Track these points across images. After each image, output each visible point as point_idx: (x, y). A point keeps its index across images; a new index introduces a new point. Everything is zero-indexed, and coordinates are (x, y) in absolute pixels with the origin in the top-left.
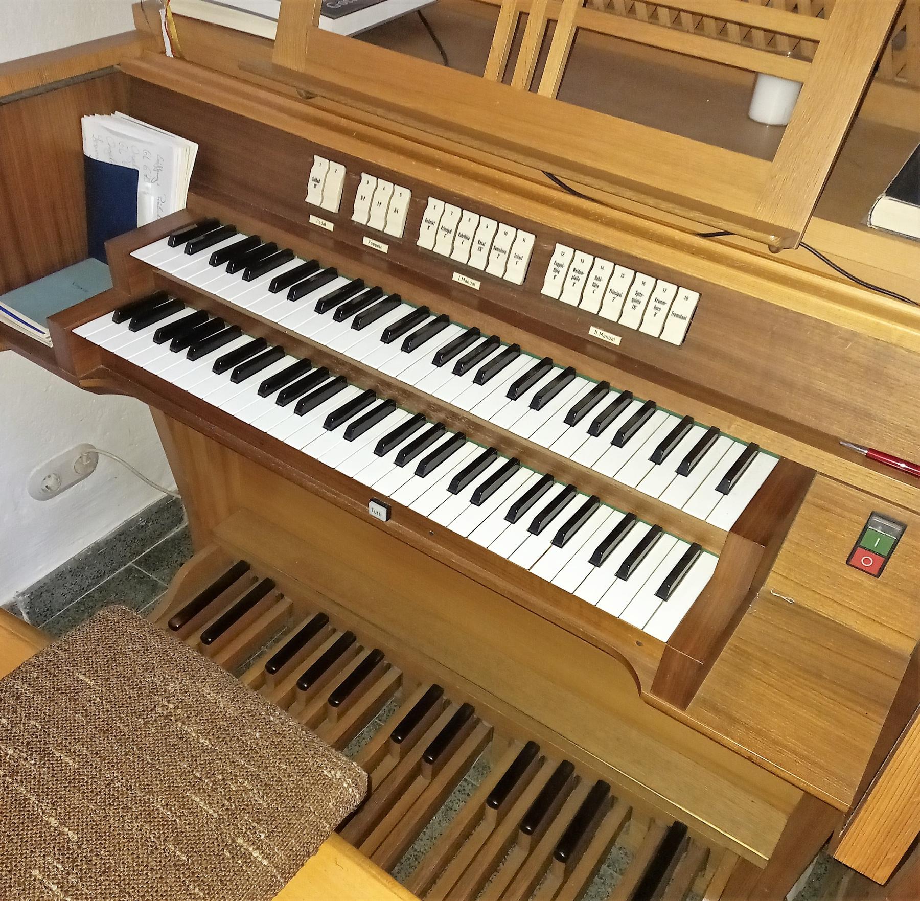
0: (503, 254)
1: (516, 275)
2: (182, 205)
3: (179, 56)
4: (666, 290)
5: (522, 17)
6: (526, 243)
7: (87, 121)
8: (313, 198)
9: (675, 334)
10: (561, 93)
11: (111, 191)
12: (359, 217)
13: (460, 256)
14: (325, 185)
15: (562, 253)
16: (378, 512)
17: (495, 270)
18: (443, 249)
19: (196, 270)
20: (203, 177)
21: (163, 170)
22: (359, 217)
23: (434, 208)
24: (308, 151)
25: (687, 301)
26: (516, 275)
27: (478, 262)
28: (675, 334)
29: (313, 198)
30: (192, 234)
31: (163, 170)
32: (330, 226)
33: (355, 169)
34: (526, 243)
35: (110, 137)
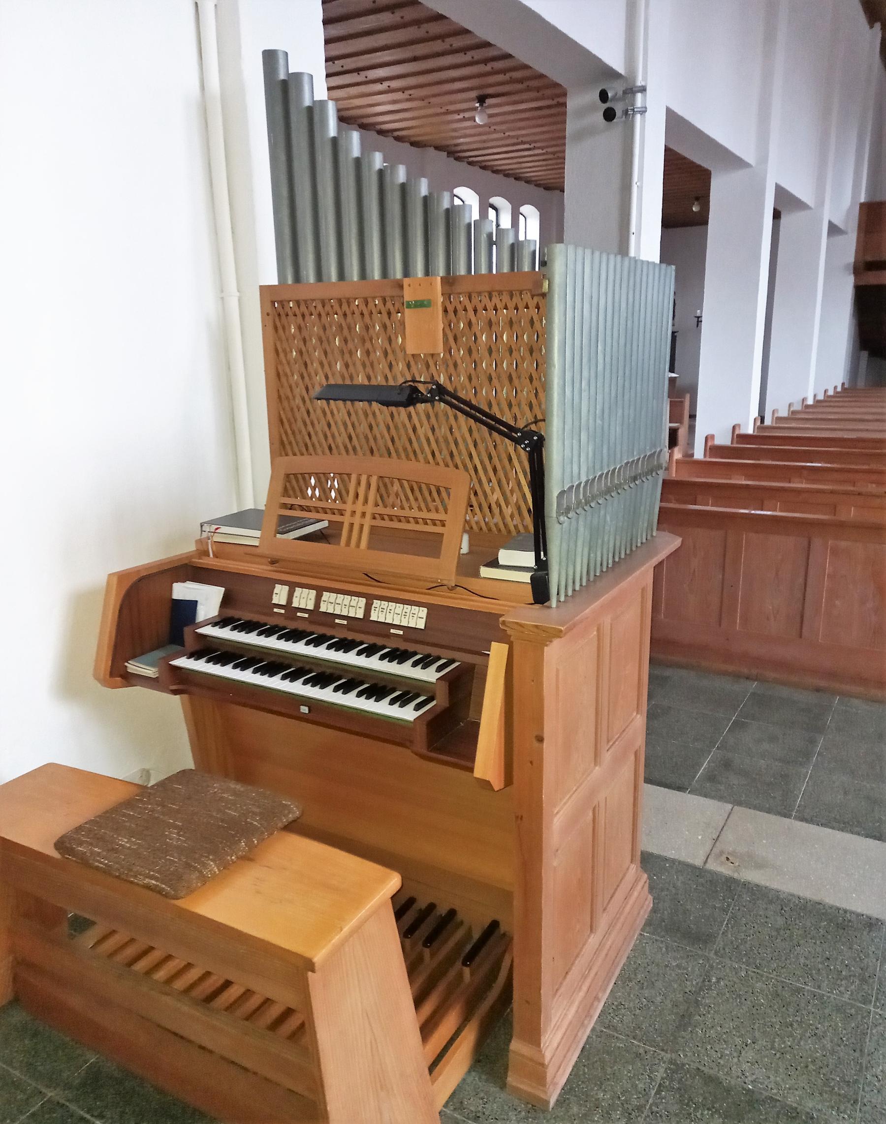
0: (353, 607)
1: (360, 615)
2: (216, 613)
3: (216, 556)
4: (415, 609)
5: (883, 407)
6: (362, 601)
7: (175, 585)
8: (275, 600)
9: (421, 625)
10: (370, 546)
11: (185, 611)
12: (295, 604)
13: (337, 612)
14: (280, 595)
15: (376, 603)
16: (304, 709)
17: (352, 615)
18: (330, 611)
19: (226, 633)
20: (226, 602)
21: (208, 599)
22: (295, 604)
23: (326, 595)
24: (272, 583)
25: (423, 612)
26: (360, 615)
27: (345, 613)
28: (421, 625)
29: (275, 600)
30: (222, 622)
31: (208, 599)
32: (283, 611)
33: (293, 586)
34: (362, 601)
35: (182, 591)
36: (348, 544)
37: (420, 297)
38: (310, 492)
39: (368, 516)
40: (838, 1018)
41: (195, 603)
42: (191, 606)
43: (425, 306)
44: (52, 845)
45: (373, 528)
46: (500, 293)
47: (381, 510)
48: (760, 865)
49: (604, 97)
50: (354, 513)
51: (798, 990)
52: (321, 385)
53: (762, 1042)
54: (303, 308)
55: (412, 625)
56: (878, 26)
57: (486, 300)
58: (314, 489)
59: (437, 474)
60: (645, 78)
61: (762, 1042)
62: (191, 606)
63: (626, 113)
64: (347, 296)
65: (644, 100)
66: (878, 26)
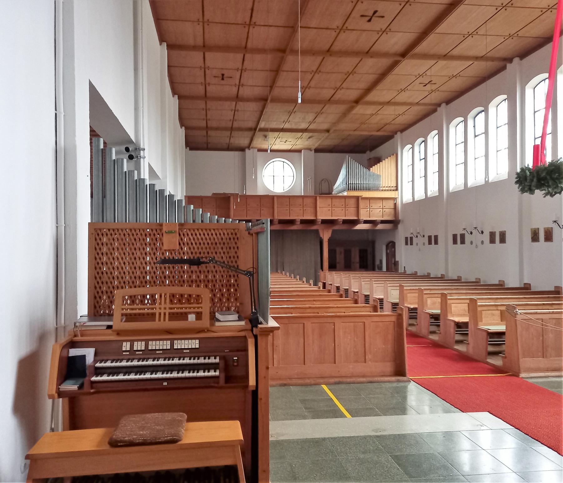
1: (169, 347)
4: (194, 341)
6: (169, 342)
9: (197, 346)
10: (169, 320)
12: (135, 349)
16: (165, 384)
20: (96, 354)
25: (197, 341)
26: (169, 347)
29: (124, 349)
31: (89, 353)
35: (73, 352)
36: (160, 320)
37: (170, 230)
38: (146, 302)
39: (167, 308)
40: (332, 463)
41: (85, 355)
42: (83, 357)
44: (107, 443)
45: (169, 314)
46: (218, 229)
48: (283, 435)
49: (127, 149)
50: (165, 308)
51: (318, 460)
52: (161, 258)
53: (318, 474)
54: (111, 231)
55: (194, 347)
58: (148, 300)
59: (194, 290)
60: (144, 145)
61: (318, 474)
62: (83, 358)
63: (137, 157)
64: (143, 228)
65: (144, 154)
66: (183, 128)
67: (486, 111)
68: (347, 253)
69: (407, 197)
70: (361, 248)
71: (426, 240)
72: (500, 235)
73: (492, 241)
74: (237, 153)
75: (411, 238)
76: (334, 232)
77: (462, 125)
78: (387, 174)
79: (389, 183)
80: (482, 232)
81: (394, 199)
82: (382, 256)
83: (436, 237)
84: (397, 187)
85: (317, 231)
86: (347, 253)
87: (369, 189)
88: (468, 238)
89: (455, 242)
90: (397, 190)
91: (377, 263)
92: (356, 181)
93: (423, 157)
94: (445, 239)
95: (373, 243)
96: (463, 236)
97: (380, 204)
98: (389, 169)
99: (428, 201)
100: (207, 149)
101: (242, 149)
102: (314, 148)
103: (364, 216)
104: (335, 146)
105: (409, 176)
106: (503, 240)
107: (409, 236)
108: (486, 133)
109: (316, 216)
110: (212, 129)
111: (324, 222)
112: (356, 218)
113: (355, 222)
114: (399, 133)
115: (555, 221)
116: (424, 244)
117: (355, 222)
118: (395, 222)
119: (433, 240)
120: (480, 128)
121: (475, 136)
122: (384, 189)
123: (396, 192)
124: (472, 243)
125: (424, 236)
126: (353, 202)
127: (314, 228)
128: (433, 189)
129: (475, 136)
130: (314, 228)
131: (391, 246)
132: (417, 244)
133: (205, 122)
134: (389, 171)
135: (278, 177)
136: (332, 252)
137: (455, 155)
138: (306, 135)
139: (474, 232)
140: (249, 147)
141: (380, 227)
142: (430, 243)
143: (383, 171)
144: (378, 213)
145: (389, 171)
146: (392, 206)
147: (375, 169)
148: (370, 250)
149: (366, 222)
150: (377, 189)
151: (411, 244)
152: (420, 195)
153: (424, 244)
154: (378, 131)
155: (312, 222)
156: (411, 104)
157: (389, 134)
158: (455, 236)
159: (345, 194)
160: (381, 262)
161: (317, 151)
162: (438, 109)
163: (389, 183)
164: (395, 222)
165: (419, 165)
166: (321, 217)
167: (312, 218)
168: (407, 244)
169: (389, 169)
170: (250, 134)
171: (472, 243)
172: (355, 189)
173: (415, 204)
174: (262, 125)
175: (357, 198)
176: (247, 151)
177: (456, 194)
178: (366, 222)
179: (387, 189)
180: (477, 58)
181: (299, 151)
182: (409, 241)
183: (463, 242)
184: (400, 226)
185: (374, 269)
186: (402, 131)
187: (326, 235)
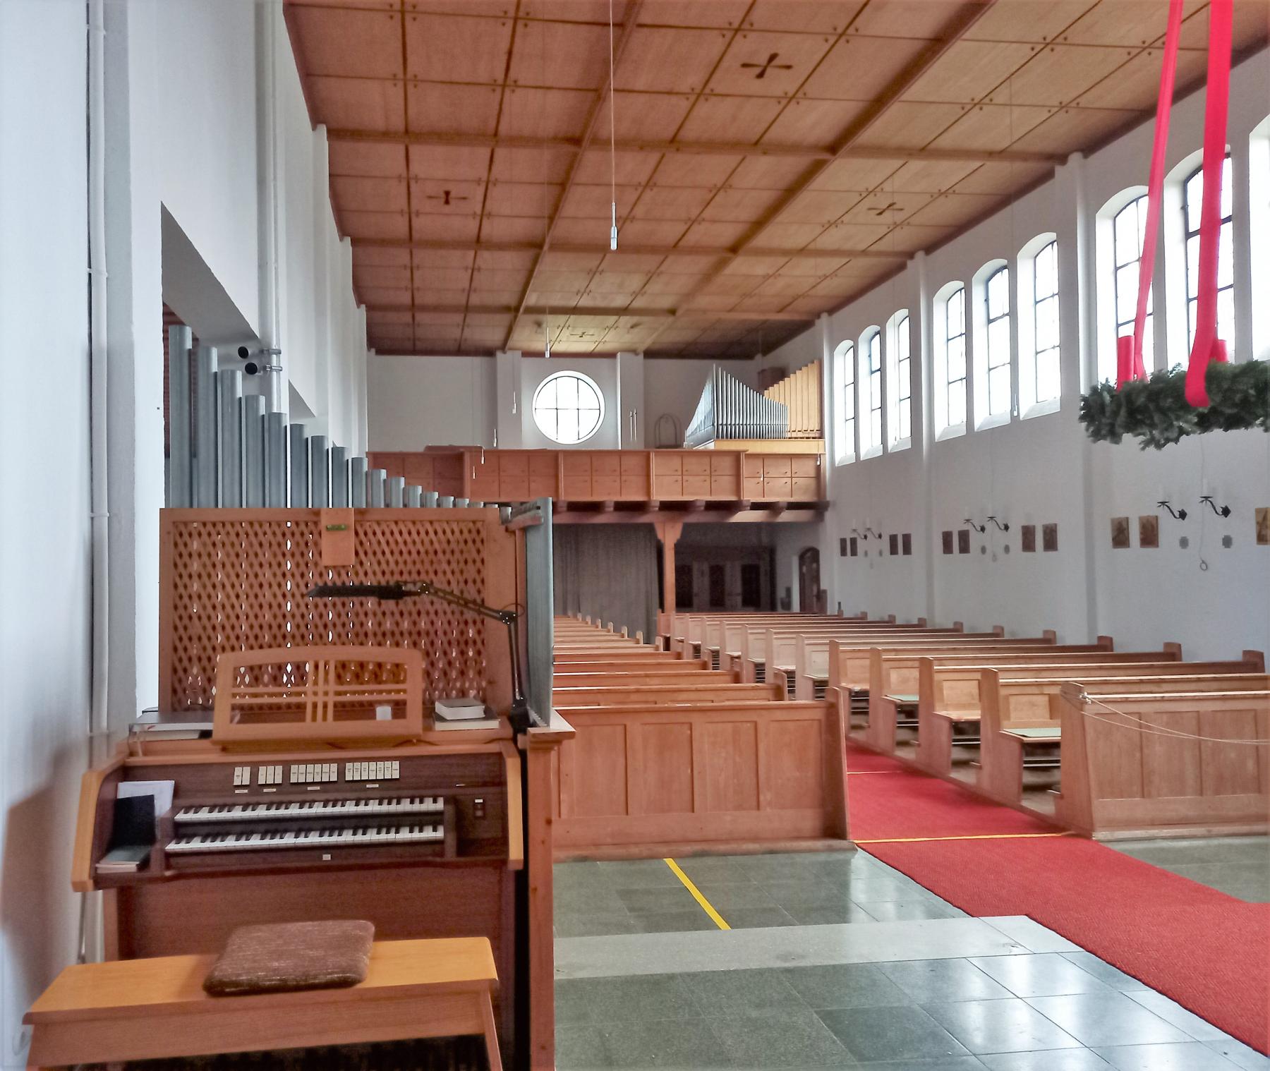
4: (388, 764)
6: (334, 767)
12: (261, 781)
17: (325, 779)
20: (177, 793)
25: (396, 764)
27: (318, 779)
29: (237, 782)
38: (285, 679)
39: (331, 694)
42: (149, 801)
43: (1265, 518)
44: (200, 988)
45: (335, 705)
47: (341, 688)
49: (243, 353)
56: (363, 307)
57: (428, 526)
58: (289, 676)
59: (387, 654)
60: (278, 343)
63: (265, 368)
65: (279, 361)
66: (363, 307)
67: (1012, 267)
68: (717, 574)
69: (843, 452)
70: (741, 564)
71: (885, 544)
72: (1045, 533)
73: (1028, 545)
74: (477, 361)
75: (854, 541)
76: (687, 527)
77: (1145, 202)
78: (799, 403)
79: (805, 422)
80: (1007, 528)
81: (816, 457)
82: (790, 578)
83: (907, 539)
84: (821, 430)
85: (650, 528)
86: (717, 574)
87: (761, 436)
88: (975, 540)
89: (947, 548)
90: (821, 437)
91: (781, 593)
92: (732, 419)
93: (876, 365)
94: (926, 544)
95: (772, 552)
96: (964, 536)
97: (785, 467)
98: (805, 393)
99: (889, 461)
100: (414, 352)
101: (489, 353)
102: (642, 347)
103: (751, 494)
104: (689, 344)
105: (848, 407)
106: (1051, 544)
107: (848, 536)
108: (1013, 314)
109: (648, 493)
110: (425, 308)
111: (667, 507)
112: (733, 498)
113: (731, 507)
114: (824, 316)
115: (1163, 503)
116: (881, 553)
117: (731, 507)
118: (817, 507)
119: (901, 545)
120: (1000, 304)
121: (990, 321)
122: (794, 435)
123: (821, 442)
124: (983, 550)
125: (880, 536)
126: (726, 464)
127: (644, 519)
128: (900, 433)
129: (990, 321)
130: (644, 519)
131: (810, 557)
132: (866, 554)
133: (409, 294)
134: (805, 398)
135: (567, 410)
136: (683, 572)
137: (947, 361)
138: (626, 320)
139: (989, 526)
140: (503, 347)
141: (786, 516)
142: (894, 551)
143: (791, 400)
144: (782, 486)
145: (805, 398)
146: (812, 473)
147: (773, 393)
148: (764, 567)
149: (756, 506)
150: (779, 436)
151: (854, 553)
152: (871, 446)
153: (881, 553)
154: (780, 311)
155: (639, 507)
156: (851, 254)
157: (804, 318)
158: (947, 537)
159: (711, 446)
160: (789, 591)
161: (650, 354)
162: (909, 263)
163: (805, 422)
164: (817, 507)
165: (869, 385)
166: (658, 496)
167: (639, 498)
168: (843, 553)
169: (805, 393)
170: (505, 318)
171: (983, 550)
172: (731, 437)
173: (862, 468)
174: (531, 299)
175: (737, 455)
176: (499, 355)
177: (949, 447)
178: (756, 506)
179: (800, 435)
180: (991, 155)
181: (611, 355)
182: (848, 547)
183: (964, 549)
184: (829, 515)
185: (772, 608)
186: (832, 311)
187: (670, 535)
